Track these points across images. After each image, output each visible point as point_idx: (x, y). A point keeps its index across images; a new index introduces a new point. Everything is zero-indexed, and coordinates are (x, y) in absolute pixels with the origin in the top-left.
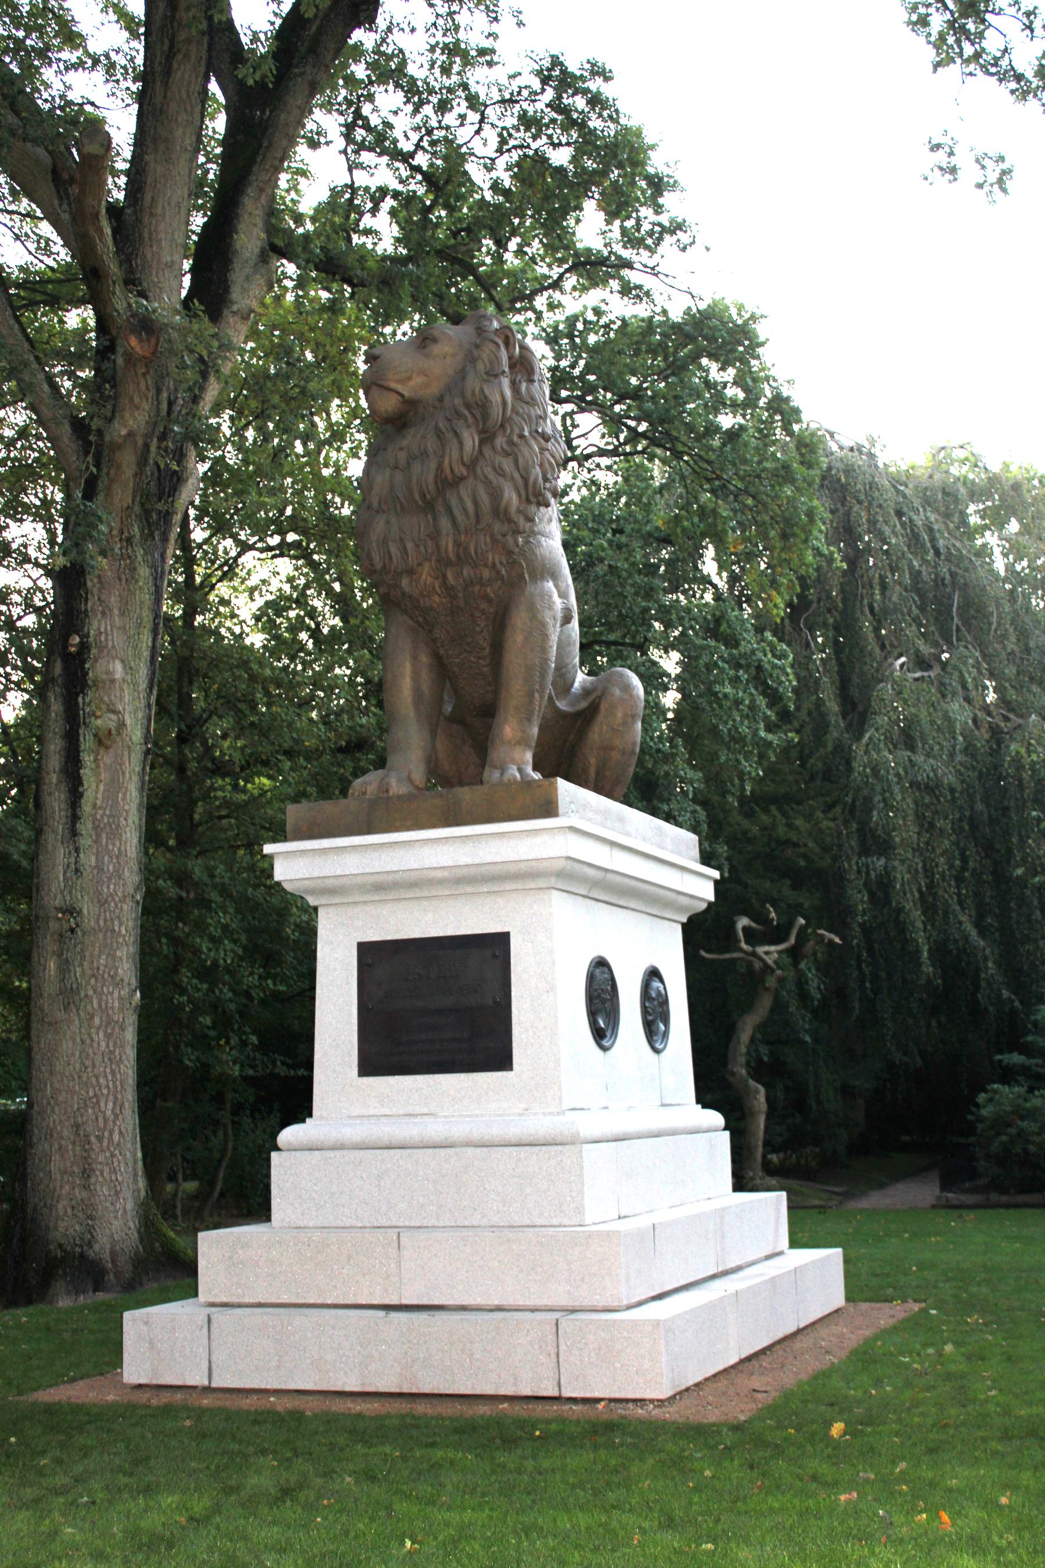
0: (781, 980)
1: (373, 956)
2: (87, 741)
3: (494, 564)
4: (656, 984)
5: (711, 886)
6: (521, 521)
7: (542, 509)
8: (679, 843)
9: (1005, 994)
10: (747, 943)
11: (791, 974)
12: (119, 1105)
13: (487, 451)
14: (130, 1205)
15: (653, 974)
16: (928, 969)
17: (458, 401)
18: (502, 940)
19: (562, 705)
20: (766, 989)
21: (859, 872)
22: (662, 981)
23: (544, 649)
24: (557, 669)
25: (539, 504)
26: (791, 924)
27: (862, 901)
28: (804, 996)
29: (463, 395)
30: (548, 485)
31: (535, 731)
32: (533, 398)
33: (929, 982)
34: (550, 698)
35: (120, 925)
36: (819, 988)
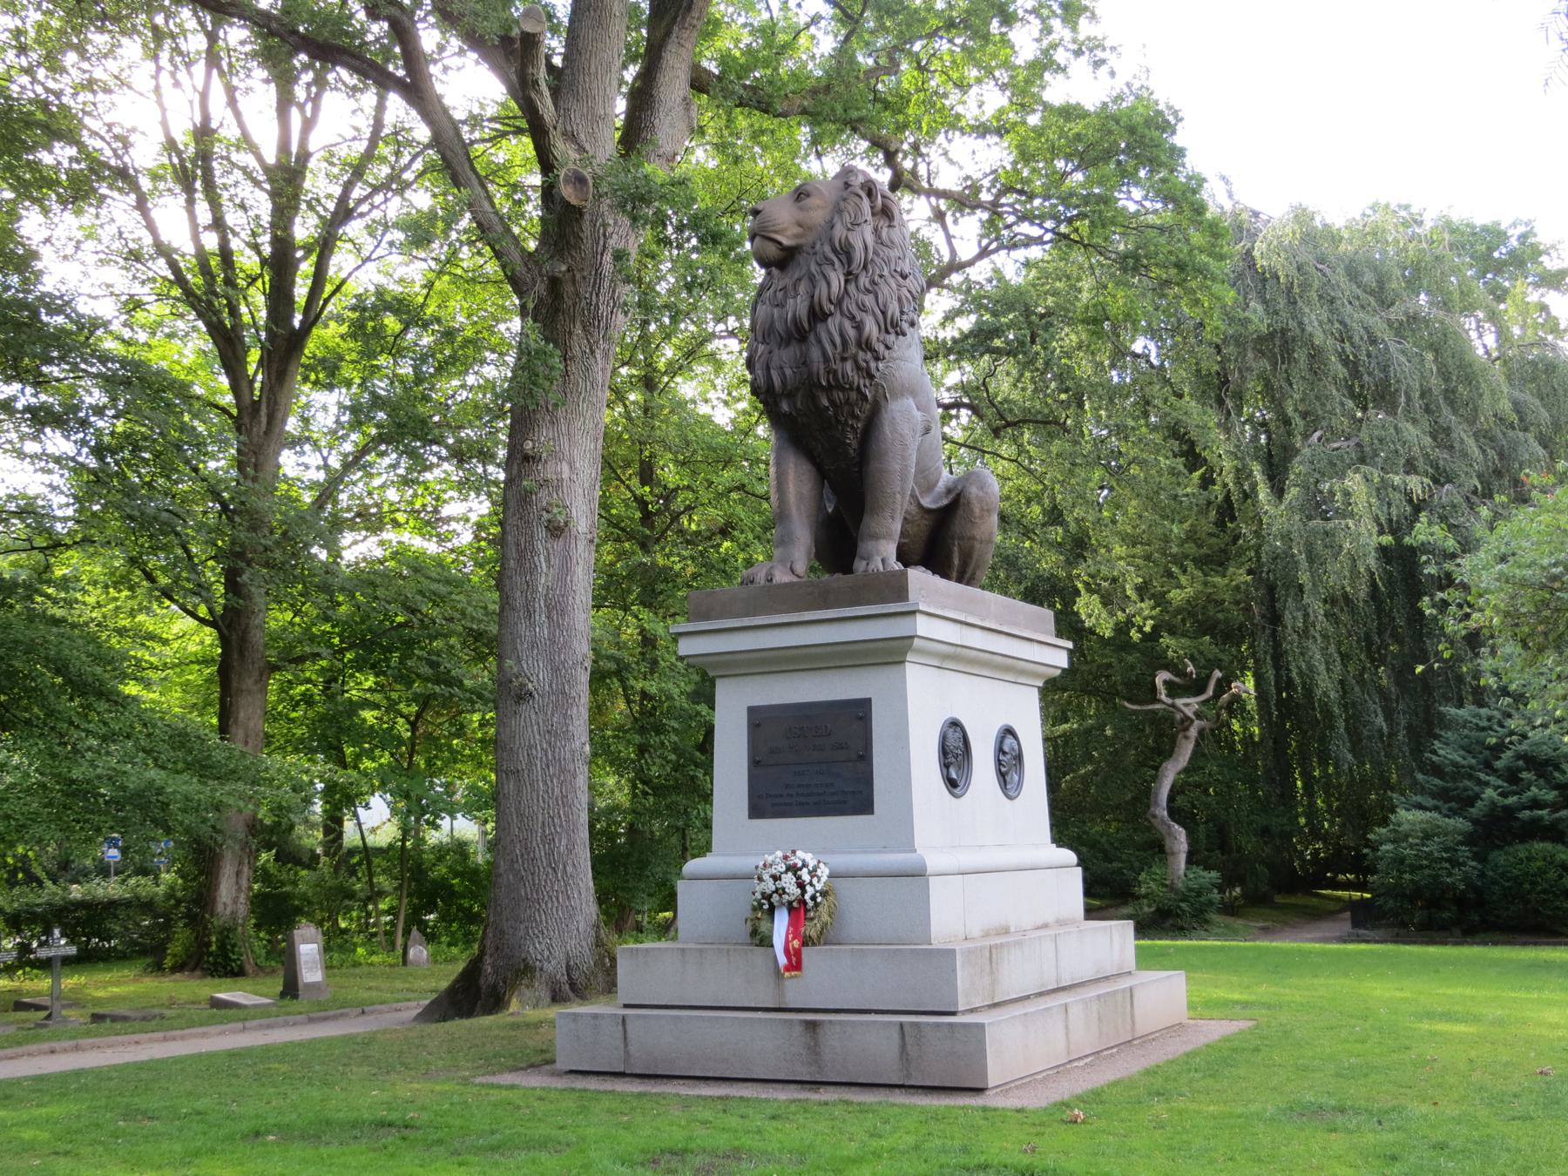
1: (758, 719)
4: (1009, 740)
13: (852, 288)
17: (827, 249)
18: (869, 700)
19: (927, 502)
26: (1209, 677)
29: (831, 241)
34: (913, 496)
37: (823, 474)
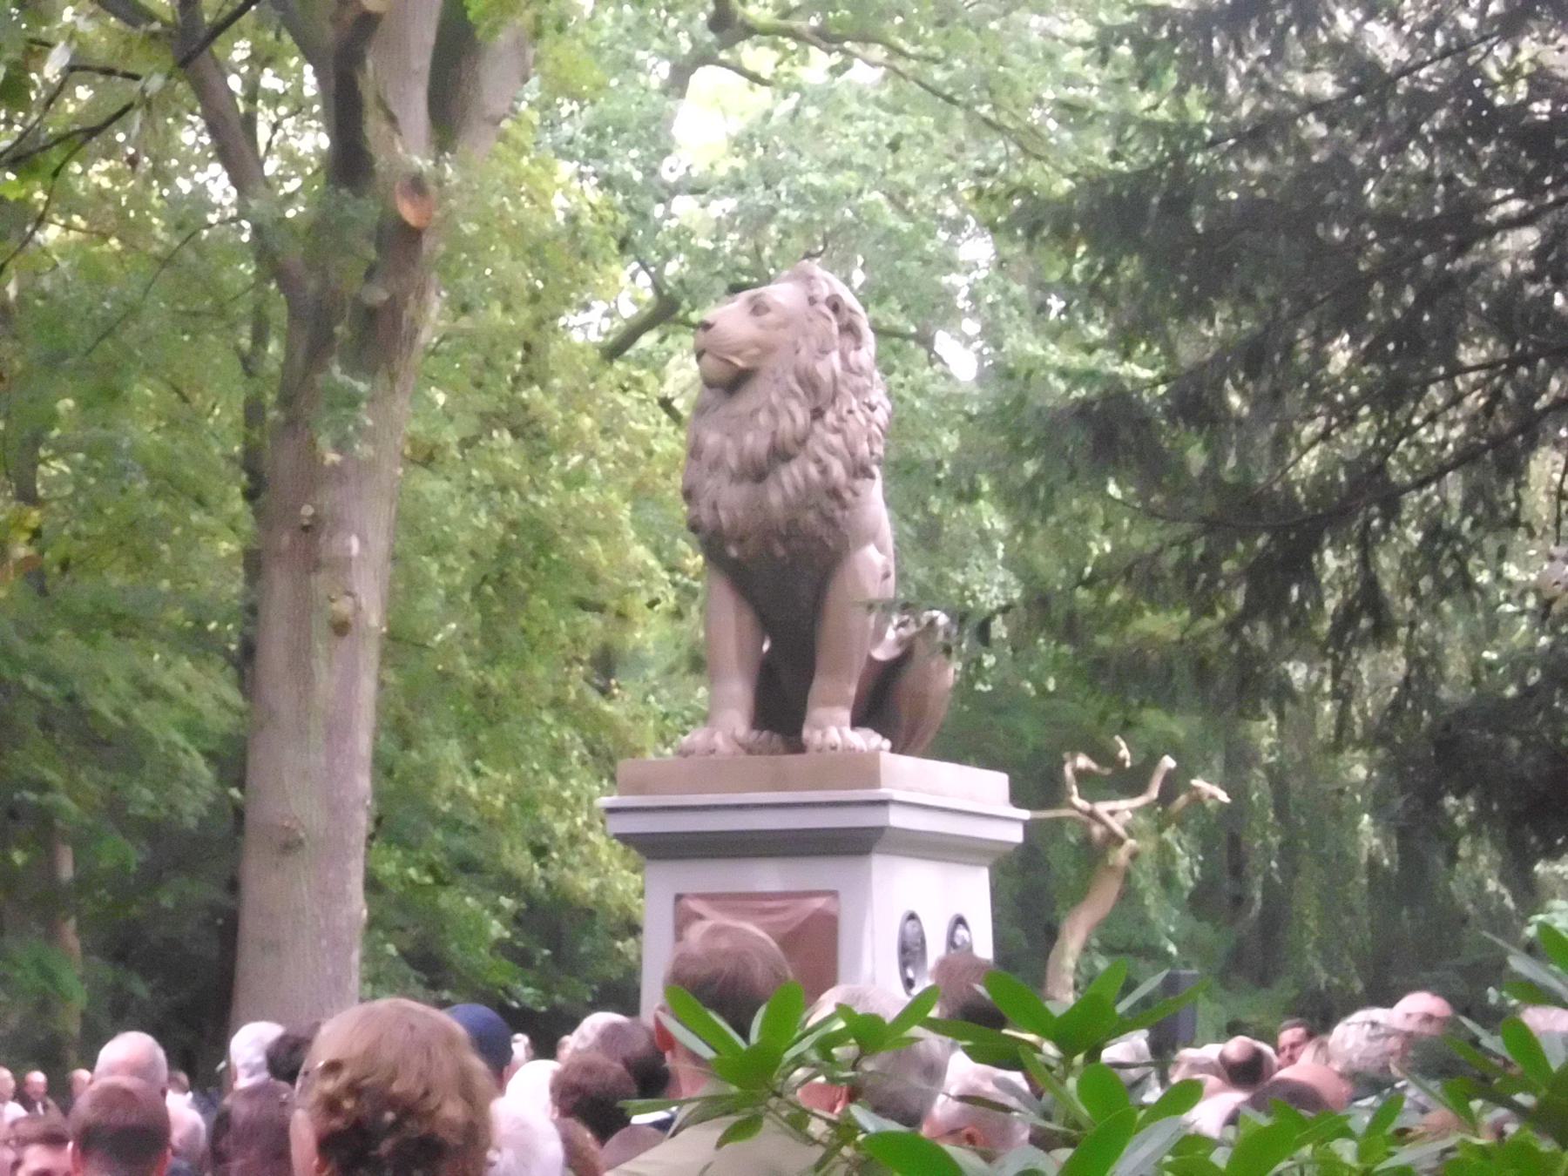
0: (1134, 856)
2: (320, 628)
4: (961, 932)
9: (1492, 885)
10: (1081, 796)
11: (1148, 846)
20: (1112, 869)
22: (966, 927)
27: (1270, 733)
28: (1167, 880)
33: (1373, 864)
36: (1192, 872)
37: (766, 623)
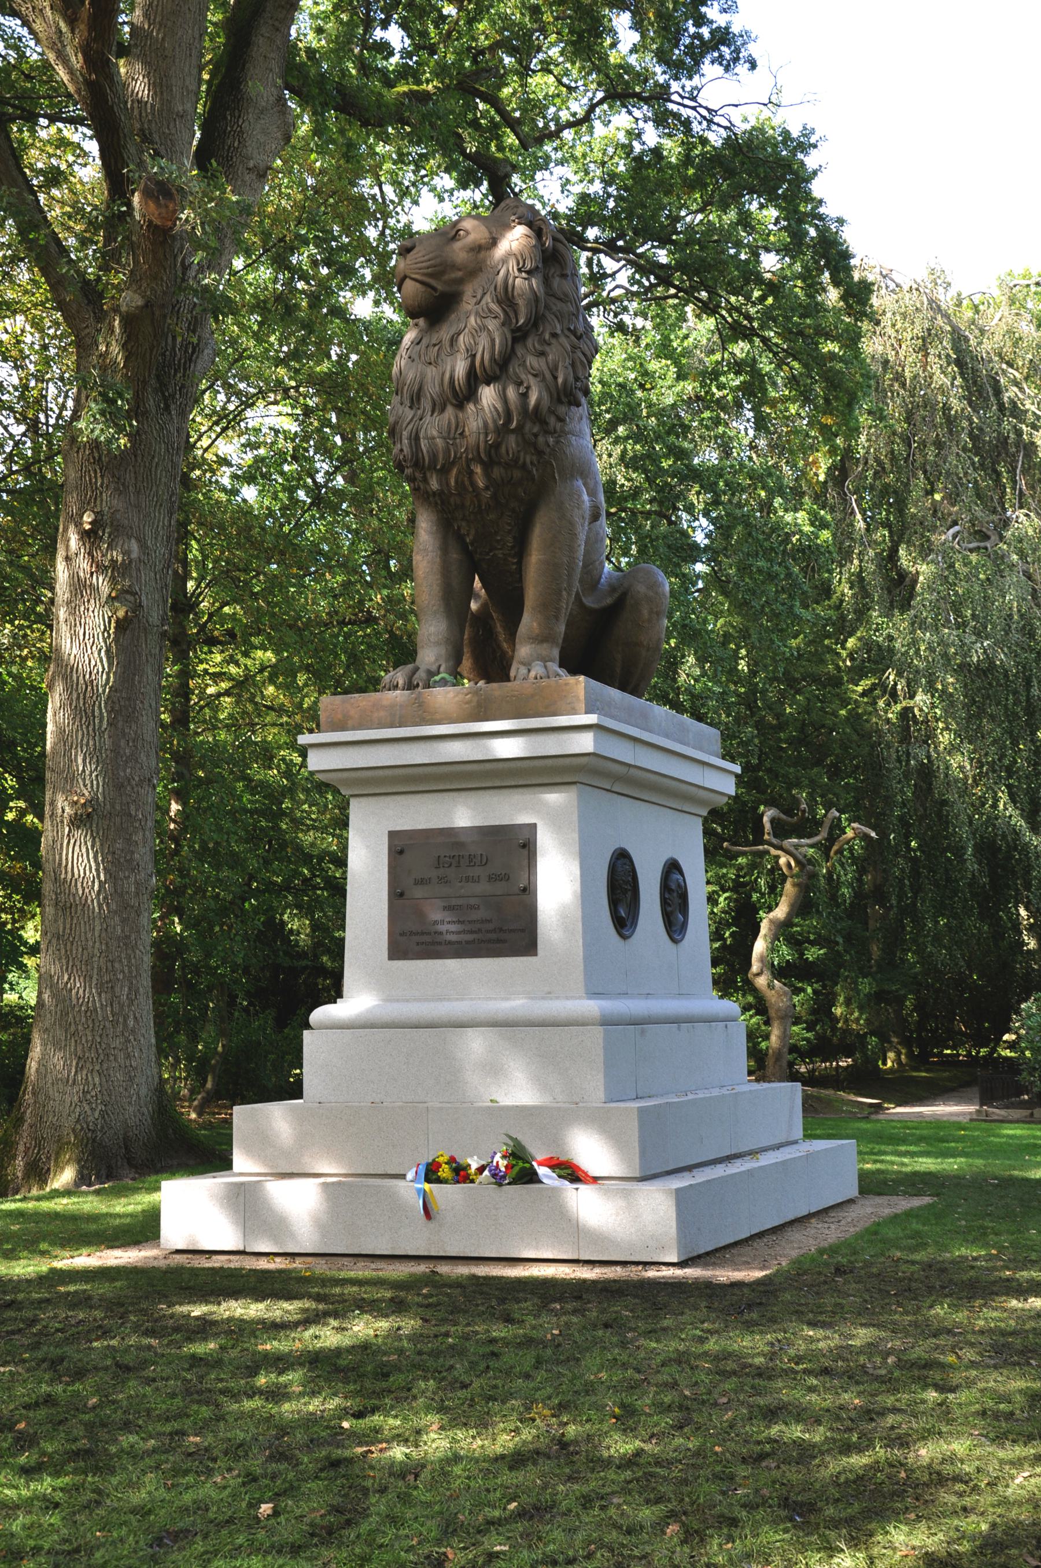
1: (402, 847)
3: (524, 463)
5: (732, 780)
6: (552, 420)
7: (573, 408)
8: (702, 740)
12: (134, 990)
13: (520, 351)
14: (144, 1091)
15: (672, 868)
16: (972, 865)
19: (589, 602)
21: (899, 760)
22: (682, 874)
23: (572, 549)
24: (585, 566)
25: (570, 404)
30: (579, 384)
31: (562, 628)
32: (566, 295)
34: (577, 594)
35: (137, 810)
